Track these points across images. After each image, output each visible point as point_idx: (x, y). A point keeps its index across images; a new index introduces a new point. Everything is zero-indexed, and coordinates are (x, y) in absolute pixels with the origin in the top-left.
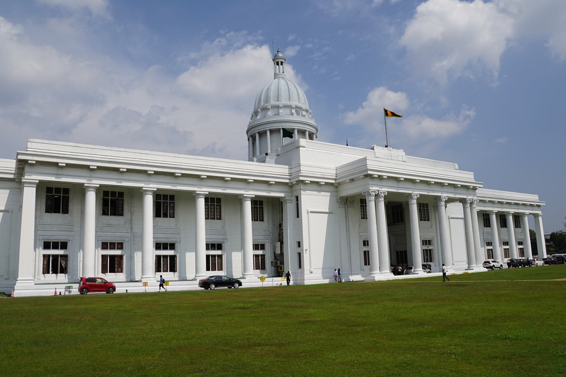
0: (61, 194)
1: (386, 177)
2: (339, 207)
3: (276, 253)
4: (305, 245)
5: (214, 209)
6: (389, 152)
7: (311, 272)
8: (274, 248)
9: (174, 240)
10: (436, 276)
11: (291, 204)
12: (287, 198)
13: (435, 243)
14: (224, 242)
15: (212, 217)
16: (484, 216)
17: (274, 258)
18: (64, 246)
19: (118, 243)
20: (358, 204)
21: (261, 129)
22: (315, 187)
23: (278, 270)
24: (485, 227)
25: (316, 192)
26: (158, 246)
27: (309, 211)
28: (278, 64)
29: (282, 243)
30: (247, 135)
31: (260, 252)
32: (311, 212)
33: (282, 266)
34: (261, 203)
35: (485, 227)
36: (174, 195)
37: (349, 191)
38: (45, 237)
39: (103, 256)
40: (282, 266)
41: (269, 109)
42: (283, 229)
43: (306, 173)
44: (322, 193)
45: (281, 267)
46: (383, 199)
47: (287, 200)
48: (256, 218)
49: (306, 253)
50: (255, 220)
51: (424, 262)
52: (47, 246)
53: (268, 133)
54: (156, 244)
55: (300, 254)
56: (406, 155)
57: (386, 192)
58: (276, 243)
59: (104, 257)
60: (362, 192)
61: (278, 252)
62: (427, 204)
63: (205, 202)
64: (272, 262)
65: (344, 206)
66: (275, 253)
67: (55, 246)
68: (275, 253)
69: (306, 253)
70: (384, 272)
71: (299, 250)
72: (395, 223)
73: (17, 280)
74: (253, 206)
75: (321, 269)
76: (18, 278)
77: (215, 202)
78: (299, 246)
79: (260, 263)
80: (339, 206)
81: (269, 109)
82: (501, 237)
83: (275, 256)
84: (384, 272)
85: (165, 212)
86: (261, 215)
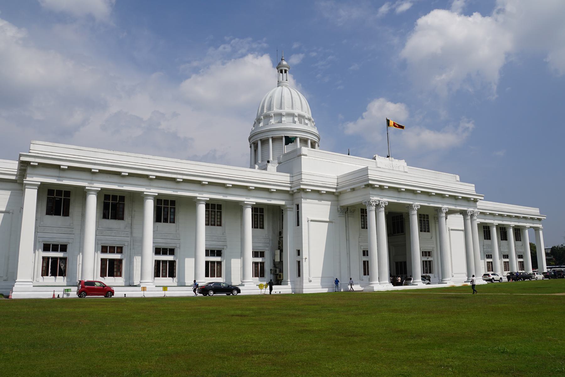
1: (387, 188)
3: (276, 261)
4: (305, 254)
5: (215, 215)
6: (391, 162)
7: (310, 281)
8: (274, 255)
9: (174, 245)
10: (435, 287)
12: (288, 206)
13: (434, 254)
14: (225, 247)
15: (213, 223)
16: (484, 228)
17: (272, 265)
18: (64, 248)
19: (118, 247)
21: (264, 136)
22: (316, 195)
23: (277, 277)
24: (485, 239)
25: (317, 201)
26: (158, 251)
27: (310, 220)
29: (281, 251)
30: (249, 142)
31: (259, 260)
32: (312, 221)
33: (281, 274)
34: (262, 210)
35: (485, 239)
37: (350, 200)
38: (46, 239)
39: (102, 260)
40: (281, 274)
41: (272, 117)
42: (282, 237)
43: (307, 181)
44: (322, 201)
45: (280, 275)
46: (384, 209)
47: (287, 208)
49: (305, 261)
50: (255, 228)
51: (424, 273)
52: (46, 248)
53: (271, 141)
55: (299, 262)
56: (407, 165)
57: (387, 202)
59: (103, 261)
61: (278, 259)
62: (428, 215)
63: (206, 209)
64: (271, 270)
66: (274, 260)
67: (55, 248)
68: (274, 260)
69: (305, 261)
73: (16, 282)
74: (253, 213)
75: (320, 278)
78: (299, 254)
81: (272, 117)
82: (501, 250)
83: (274, 264)
85: (166, 217)
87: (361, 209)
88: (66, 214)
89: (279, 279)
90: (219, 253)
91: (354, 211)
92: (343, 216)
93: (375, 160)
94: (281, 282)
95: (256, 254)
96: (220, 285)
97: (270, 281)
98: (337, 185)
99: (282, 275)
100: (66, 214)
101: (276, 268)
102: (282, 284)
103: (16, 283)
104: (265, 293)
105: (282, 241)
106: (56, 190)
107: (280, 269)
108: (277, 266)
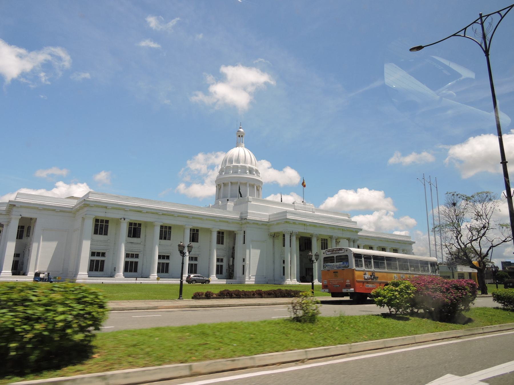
0: (104, 223)
2: (269, 239)
3: (230, 264)
4: (247, 262)
8: (229, 261)
11: (278, 240)
17: (228, 266)
18: (103, 254)
20: (281, 237)
23: (230, 275)
28: (239, 136)
29: (234, 258)
31: (220, 264)
33: (233, 272)
34: (223, 233)
36: (141, 224)
37: (276, 229)
40: (233, 272)
42: (234, 250)
45: (232, 273)
48: (130, 235)
54: (127, 254)
58: (230, 258)
60: (333, 236)
61: (231, 263)
62: (327, 239)
64: (227, 270)
65: (272, 238)
66: (229, 264)
68: (229, 264)
70: (212, 276)
71: (283, 265)
72: (306, 250)
73: (1, 273)
76: (2, 271)
77: (100, 222)
78: (244, 261)
79: (219, 271)
80: (270, 238)
83: (229, 266)
84: (212, 276)
85: (165, 236)
86: (169, 236)
87: (283, 235)
88: (106, 234)
89: (232, 275)
90: (196, 259)
91: (278, 236)
92: (272, 238)
93: (294, 204)
94: (232, 277)
95: (218, 260)
96: (282, 232)
97: (327, 290)
98: (269, 220)
99: (233, 273)
100: (106, 234)
101: (230, 269)
102: (233, 279)
103: (1, 273)
104: (106, 216)
105: (234, 252)
106: (101, 220)
107: (232, 270)
108: (231, 267)
